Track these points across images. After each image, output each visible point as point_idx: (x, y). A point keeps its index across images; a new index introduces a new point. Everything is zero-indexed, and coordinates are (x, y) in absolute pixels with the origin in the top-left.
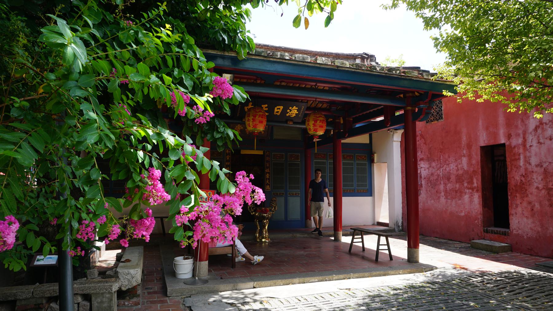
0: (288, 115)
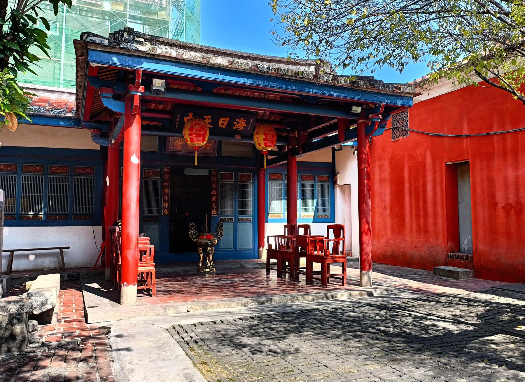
0: (234, 128)
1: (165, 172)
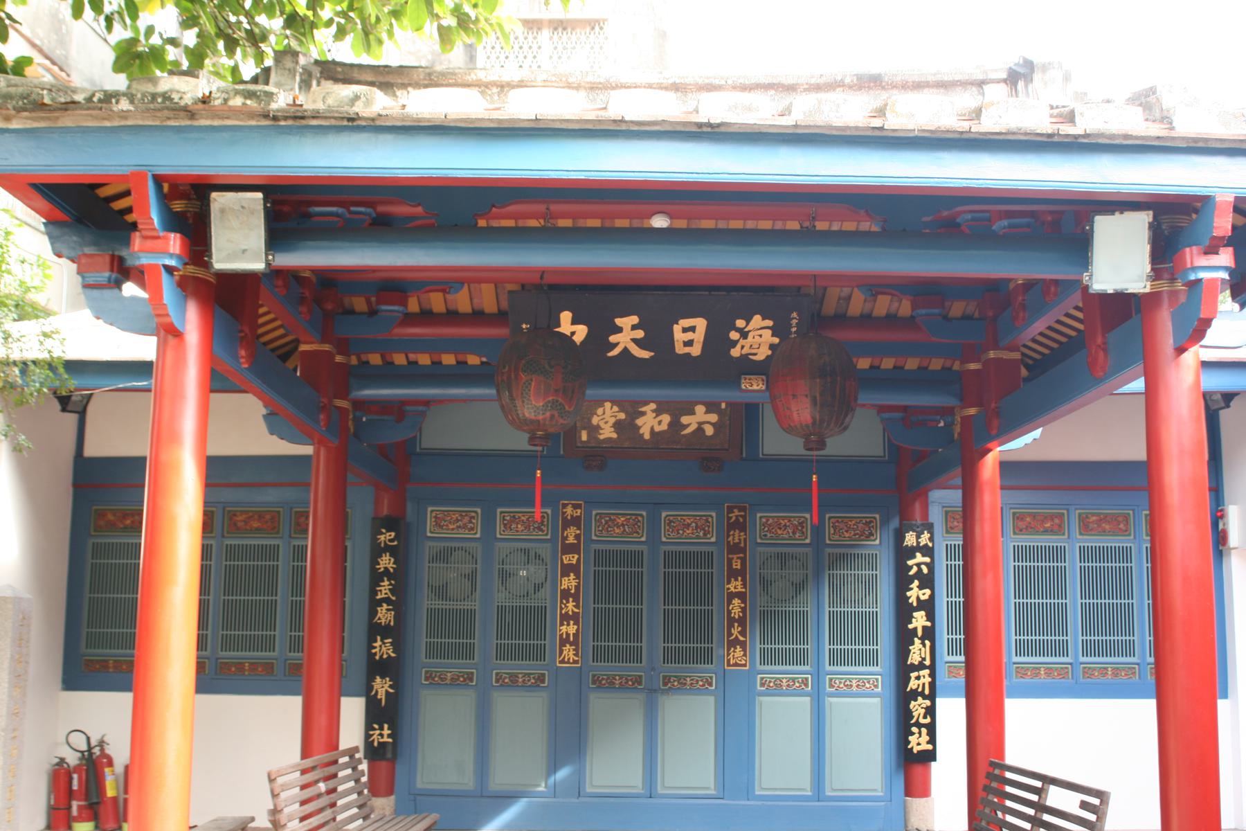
0: (735, 352)
1: (564, 519)
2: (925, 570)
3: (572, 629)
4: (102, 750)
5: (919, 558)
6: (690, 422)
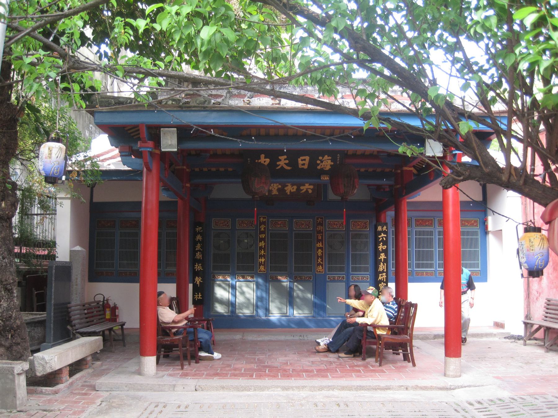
0: (319, 167)
2: (385, 239)
3: (263, 260)
4: (107, 302)
5: (383, 235)
6: (304, 188)
